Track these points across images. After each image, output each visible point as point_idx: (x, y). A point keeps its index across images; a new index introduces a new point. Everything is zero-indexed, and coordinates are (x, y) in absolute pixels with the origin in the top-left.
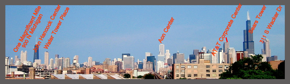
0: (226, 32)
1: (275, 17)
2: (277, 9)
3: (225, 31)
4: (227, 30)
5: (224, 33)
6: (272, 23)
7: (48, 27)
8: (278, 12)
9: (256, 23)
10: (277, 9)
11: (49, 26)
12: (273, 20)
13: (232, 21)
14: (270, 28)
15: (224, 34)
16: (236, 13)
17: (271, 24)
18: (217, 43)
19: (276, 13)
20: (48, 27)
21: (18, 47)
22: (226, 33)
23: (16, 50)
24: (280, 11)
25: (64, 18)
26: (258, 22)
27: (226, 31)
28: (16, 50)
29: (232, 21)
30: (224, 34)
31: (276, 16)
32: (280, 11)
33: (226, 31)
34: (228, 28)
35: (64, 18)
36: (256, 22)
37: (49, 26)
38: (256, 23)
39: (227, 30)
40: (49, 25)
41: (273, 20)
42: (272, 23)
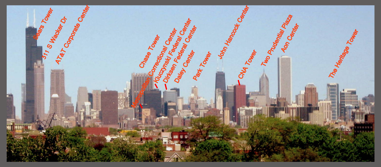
0: (71, 37)
1: (59, 30)
2: (61, 21)
3: (71, 36)
4: (73, 35)
5: (69, 39)
6: (56, 36)
7: (235, 31)
8: (62, 24)
9: (41, 28)
10: (61, 21)
11: (235, 29)
12: (57, 33)
13: (78, 25)
14: (53, 42)
15: (70, 39)
16: (83, 16)
17: (54, 38)
18: (62, 50)
19: (60, 25)
20: (235, 31)
21: (231, 37)
22: (72, 39)
23: (268, 58)
24: (64, 23)
25: (272, 52)
26: (43, 28)
27: (72, 36)
28: (268, 58)
29: (78, 25)
30: (70, 39)
31: (59, 29)
32: (64, 23)
33: (72, 36)
34: (74, 33)
35: (272, 52)
36: (42, 27)
37: (235, 29)
38: (41, 28)
39: (73, 35)
40: (236, 28)
41: (57, 33)
42: (56, 36)
